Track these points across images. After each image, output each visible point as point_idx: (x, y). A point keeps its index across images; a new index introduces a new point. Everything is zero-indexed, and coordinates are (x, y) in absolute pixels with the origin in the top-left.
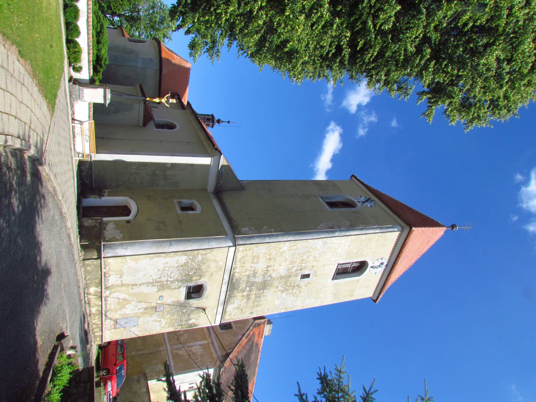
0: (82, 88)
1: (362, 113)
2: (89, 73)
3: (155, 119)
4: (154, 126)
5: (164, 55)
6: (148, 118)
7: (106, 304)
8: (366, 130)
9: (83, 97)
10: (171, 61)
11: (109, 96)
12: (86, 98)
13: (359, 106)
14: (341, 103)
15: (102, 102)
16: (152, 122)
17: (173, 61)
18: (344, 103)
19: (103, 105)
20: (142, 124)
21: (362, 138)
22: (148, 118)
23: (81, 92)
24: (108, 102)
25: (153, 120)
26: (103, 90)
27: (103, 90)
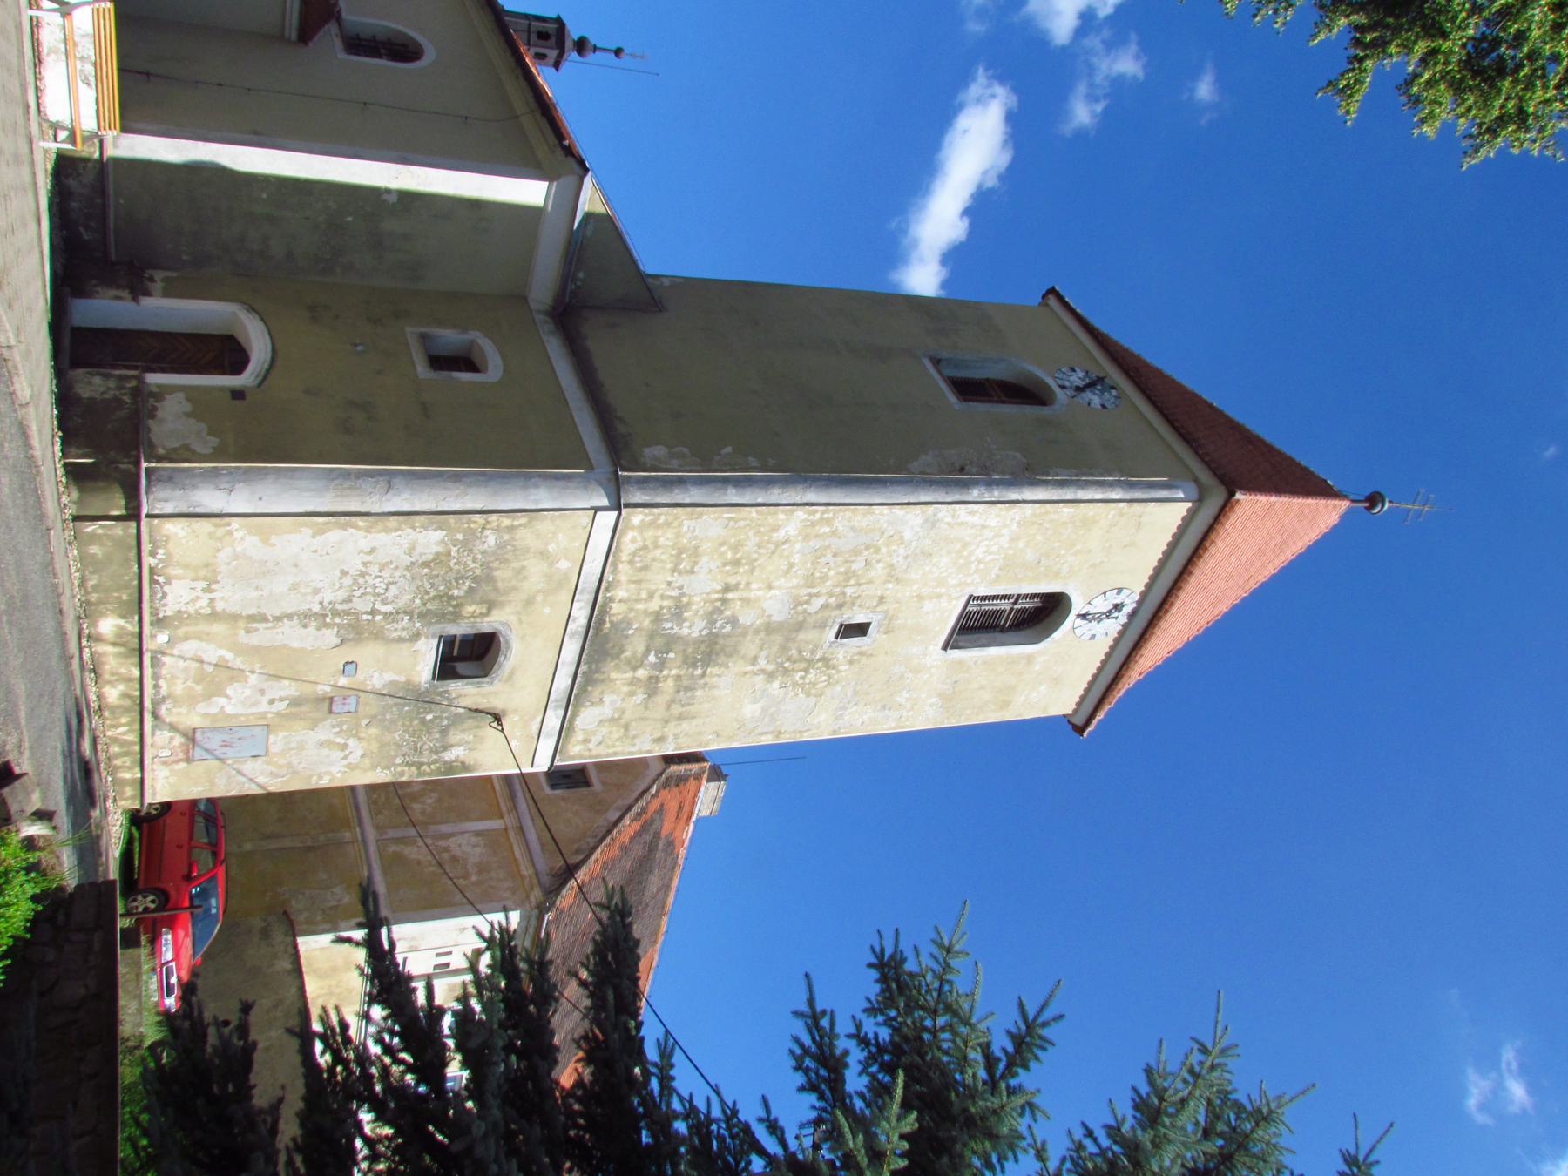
1: (1093, 42)
3: (345, 15)
4: (338, 43)
8: (1099, 108)
16: (332, 28)
20: (294, 35)
21: (1081, 134)
25: (339, 19)
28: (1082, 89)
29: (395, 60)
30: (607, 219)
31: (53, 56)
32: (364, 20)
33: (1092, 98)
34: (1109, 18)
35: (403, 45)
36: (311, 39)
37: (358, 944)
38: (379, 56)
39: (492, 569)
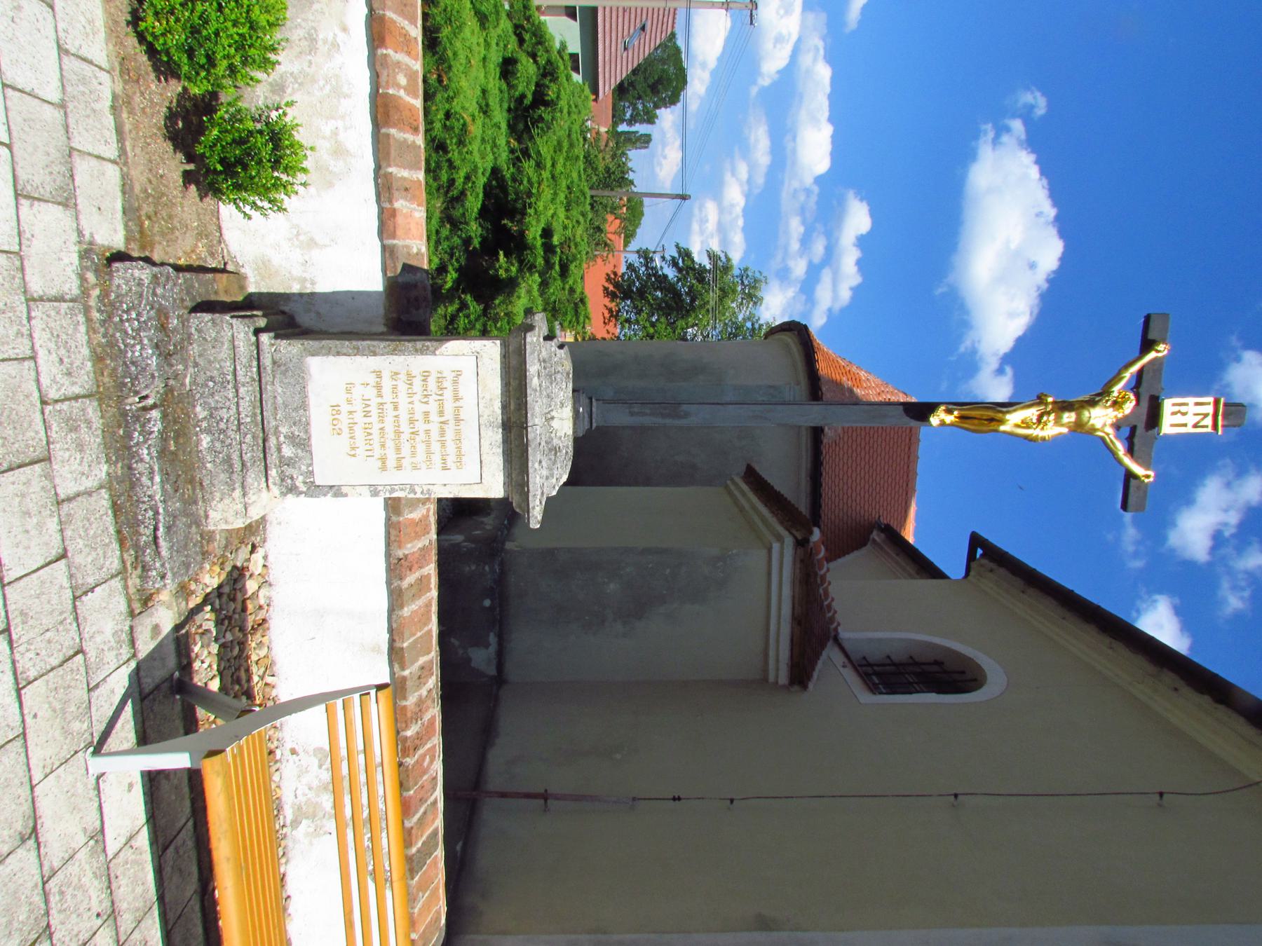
0: (290, 349)
1: (1227, 550)
2: (387, 223)
3: (844, 634)
4: (849, 675)
5: (823, 368)
6: (812, 631)
7: (736, 502)
8: (1246, 594)
9: (303, 443)
10: (851, 391)
11: (556, 420)
12: (328, 455)
13: (1218, 539)
14: (1162, 539)
15: (493, 487)
16: (831, 654)
17: (858, 392)
18: (1173, 539)
19: (506, 512)
20: (783, 679)
21: (1238, 616)
22: (812, 631)
23: (277, 390)
24: (548, 477)
25: (836, 640)
26: (491, 350)
27: (491, 350)
28: (1225, 584)
29: (940, 691)
30: (196, 731)
31: (305, 825)
32: (870, 635)
33: (1235, 588)
34: (1233, 536)
35: (936, 663)
36: (809, 677)
37: (388, 252)
38: (907, 689)
39: (221, 87)
